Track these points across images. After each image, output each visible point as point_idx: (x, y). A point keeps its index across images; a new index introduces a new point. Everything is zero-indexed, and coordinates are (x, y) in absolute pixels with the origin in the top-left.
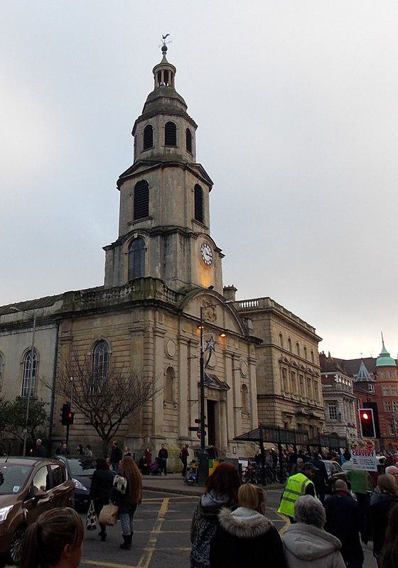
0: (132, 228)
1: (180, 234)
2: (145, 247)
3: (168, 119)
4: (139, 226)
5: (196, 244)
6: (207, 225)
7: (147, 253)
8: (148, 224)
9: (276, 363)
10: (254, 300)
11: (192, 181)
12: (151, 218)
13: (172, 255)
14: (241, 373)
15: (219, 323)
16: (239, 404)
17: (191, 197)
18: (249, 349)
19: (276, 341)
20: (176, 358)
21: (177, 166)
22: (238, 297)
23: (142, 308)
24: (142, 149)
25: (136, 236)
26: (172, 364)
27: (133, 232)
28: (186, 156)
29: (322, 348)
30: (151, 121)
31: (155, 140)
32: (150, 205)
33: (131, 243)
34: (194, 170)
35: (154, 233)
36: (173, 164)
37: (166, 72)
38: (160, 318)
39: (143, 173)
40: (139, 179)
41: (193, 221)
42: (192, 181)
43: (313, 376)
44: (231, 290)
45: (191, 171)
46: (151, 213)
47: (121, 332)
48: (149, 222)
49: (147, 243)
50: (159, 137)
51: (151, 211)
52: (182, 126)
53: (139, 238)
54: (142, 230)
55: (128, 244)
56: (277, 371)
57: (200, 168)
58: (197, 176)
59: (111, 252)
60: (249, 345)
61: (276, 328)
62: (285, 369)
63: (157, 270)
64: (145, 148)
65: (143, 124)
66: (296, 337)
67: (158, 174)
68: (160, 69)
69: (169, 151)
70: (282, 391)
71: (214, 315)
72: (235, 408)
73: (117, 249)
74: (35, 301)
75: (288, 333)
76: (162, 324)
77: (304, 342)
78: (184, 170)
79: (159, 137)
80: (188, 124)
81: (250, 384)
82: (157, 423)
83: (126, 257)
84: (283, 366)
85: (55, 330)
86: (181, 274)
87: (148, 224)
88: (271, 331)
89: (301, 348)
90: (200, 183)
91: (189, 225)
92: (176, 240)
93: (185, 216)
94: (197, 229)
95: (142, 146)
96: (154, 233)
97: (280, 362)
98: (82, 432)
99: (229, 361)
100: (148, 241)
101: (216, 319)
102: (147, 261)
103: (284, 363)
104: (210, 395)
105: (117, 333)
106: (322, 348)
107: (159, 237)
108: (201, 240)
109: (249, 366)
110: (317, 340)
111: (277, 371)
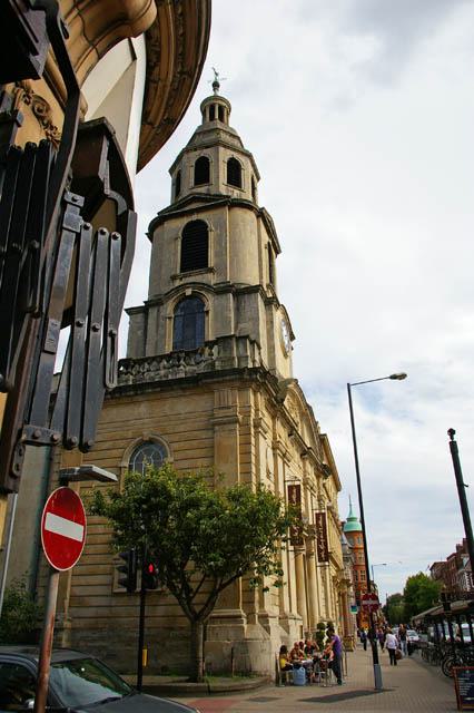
0: (178, 283)
23: (238, 384)
24: (192, 184)
25: (189, 292)
27: (184, 286)
33: (180, 302)
37: (221, 109)
39: (198, 210)
40: (195, 217)
46: (211, 263)
47: (196, 426)
48: (210, 276)
53: (194, 296)
59: (140, 317)
64: (182, 270)
65: (195, 156)
68: (212, 102)
73: (153, 313)
74: (352, 692)
78: (258, 217)
83: (170, 325)
95: (193, 180)
98: (105, 612)
100: (210, 302)
105: (182, 428)
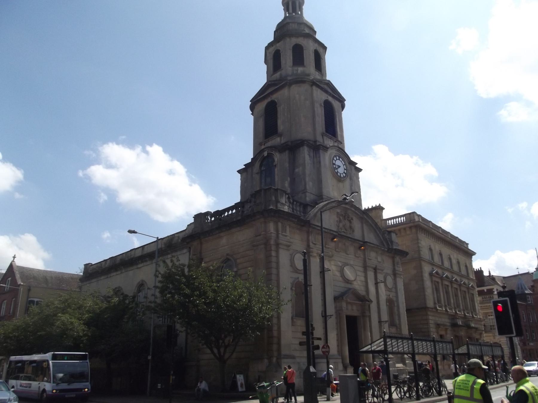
0: (263, 147)
1: (308, 146)
2: (274, 164)
3: (294, 41)
4: (269, 144)
5: (326, 157)
6: (339, 139)
7: (276, 170)
8: (276, 141)
9: (426, 276)
10: (400, 216)
11: (320, 96)
12: (280, 135)
13: (301, 168)
14: (386, 286)
15: (357, 235)
16: (385, 317)
17: (320, 112)
18: (393, 262)
19: (425, 253)
20: (394, 290)
21: (303, 82)
22: (386, 215)
25: (265, 154)
26: (392, 295)
28: (315, 75)
29: (476, 264)
30: (279, 46)
31: (283, 62)
32: (279, 122)
34: (322, 85)
35: (282, 149)
36: (300, 81)
38: (284, 230)
40: (269, 100)
41: (323, 135)
42: (320, 96)
43: (460, 285)
44: (379, 209)
45: (318, 86)
49: (276, 159)
50: (287, 60)
51: (281, 127)
52: (309, 48)
54: (271, 148)
55: (259, 163)
56: (428, 283)
57: (329, 84)
58: (326, 92)
59: (245, 174)
60: (393, 258)
61: (425, 242)
62: (438, 282)
63: (287, 184)
66: (447, 251)
67: (285, 92)
69: (297, 70)
70: (435, 303)
71: (351, 227)
72: (380, 322)
75: (437, 247)
76: (286, 236)
77: (455, 256)
78: (312, 86)
79: (287, 60)
80: (316, 45)
81: (397, 297)
82: (283, 342)
84: (435, 279)
85: (188, 254)
86: (310, 186)
87: (276, 141)
88: (420, 245)
89: (454, 261)
90: (330, 99)
91: (319, 139)
92: (305, 154)
93: (314, 129)
94: (329, 142)
96: (282, 149)
97: (431, 274)
99: (371, 274)
100: (277, 157)
101: (353, 231)
102: (276, 177)
103: (436, 277)
104: (354, 311)
106: (476, 264)
107: (287, 152)
108: (332, 152)
109: (395, 280)
110: (470, 254)
111: (428, 283)
